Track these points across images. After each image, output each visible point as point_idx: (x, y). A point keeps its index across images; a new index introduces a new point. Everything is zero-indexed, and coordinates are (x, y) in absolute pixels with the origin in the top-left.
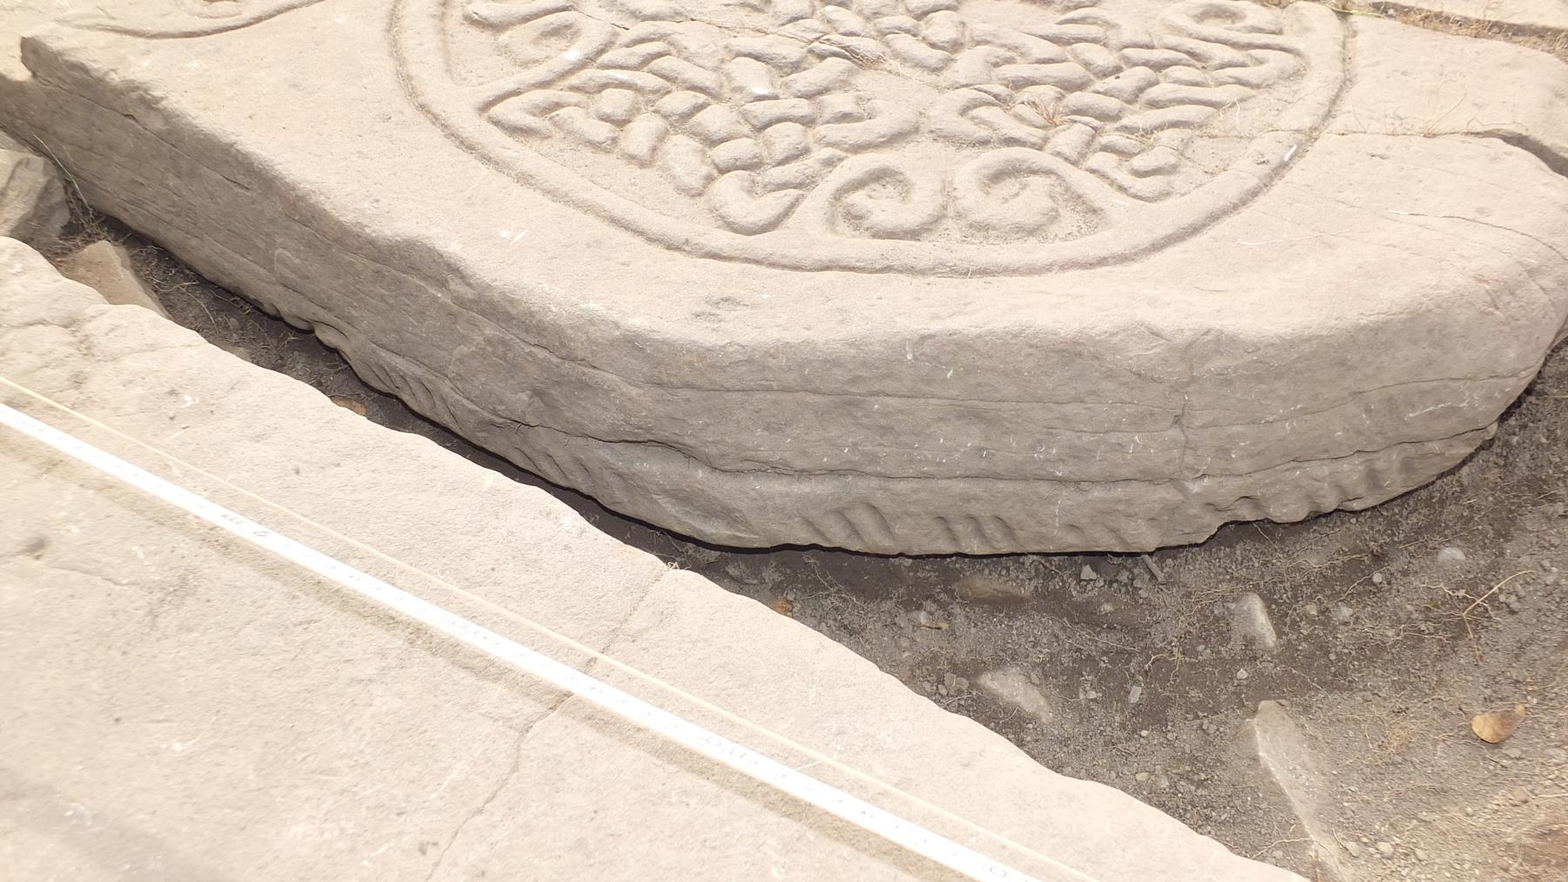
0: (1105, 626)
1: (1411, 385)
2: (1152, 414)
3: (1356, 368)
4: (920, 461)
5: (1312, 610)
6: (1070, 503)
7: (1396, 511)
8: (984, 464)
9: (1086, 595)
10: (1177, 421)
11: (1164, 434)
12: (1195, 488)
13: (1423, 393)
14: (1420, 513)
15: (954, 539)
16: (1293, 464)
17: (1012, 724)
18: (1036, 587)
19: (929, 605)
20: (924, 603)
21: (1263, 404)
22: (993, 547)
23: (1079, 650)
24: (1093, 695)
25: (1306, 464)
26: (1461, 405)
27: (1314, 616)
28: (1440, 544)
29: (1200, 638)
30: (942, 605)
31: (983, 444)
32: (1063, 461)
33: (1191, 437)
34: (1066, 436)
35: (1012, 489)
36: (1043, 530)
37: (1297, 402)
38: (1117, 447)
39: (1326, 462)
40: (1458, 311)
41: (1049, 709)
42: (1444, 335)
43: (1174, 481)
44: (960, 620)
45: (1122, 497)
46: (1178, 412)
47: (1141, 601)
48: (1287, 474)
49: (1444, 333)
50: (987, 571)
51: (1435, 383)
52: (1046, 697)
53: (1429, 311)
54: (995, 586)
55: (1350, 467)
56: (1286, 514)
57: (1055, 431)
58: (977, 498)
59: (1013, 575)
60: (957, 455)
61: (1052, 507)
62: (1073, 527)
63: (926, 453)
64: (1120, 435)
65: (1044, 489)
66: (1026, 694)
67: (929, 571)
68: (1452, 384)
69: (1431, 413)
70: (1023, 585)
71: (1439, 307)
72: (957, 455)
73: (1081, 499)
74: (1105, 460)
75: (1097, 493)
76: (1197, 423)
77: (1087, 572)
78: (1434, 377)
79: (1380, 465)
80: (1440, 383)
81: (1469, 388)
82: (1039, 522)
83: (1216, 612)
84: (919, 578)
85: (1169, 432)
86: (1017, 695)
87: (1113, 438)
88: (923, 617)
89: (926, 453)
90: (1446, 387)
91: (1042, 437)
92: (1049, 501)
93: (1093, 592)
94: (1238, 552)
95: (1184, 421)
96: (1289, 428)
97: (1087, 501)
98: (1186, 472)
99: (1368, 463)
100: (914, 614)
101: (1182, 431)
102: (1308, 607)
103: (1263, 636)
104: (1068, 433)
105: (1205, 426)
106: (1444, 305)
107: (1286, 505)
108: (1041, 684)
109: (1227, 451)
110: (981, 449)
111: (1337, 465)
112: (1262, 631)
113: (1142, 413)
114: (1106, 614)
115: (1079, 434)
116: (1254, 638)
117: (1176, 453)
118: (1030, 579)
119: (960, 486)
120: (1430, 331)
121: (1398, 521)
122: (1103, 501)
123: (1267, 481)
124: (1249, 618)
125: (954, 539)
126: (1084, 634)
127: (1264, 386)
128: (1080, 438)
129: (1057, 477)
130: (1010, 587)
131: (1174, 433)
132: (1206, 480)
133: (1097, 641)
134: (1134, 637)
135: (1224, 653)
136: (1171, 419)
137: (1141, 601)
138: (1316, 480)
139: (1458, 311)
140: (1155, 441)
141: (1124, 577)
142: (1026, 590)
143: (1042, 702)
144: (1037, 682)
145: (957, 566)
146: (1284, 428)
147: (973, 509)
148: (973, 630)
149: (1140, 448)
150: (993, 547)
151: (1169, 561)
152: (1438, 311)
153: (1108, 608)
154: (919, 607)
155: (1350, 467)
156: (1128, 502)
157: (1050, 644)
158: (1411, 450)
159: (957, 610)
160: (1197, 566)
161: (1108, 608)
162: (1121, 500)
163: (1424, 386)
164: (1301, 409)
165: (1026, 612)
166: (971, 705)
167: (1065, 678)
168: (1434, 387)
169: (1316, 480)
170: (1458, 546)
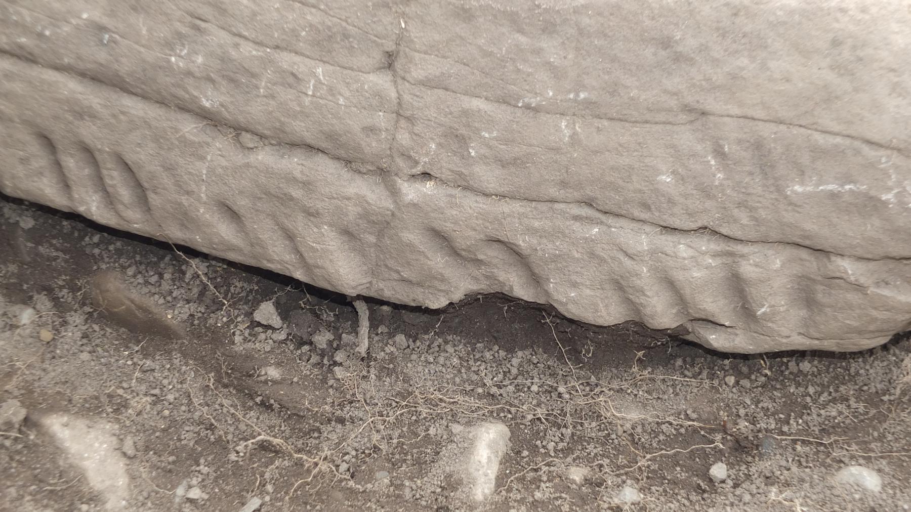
0: (258, 400)
1: (795, 131)
2: (346, 36)
3: (690, 61)
4: (16, 24)
5: (577, 474)
6: (224, 163)
7: (811, 390)
8: (102, 56)
9: (250, 345)
10: (389, 62)
11: (363, 77)
12: (411, 192)
13: (818, 152)
14: (849, 406)
15: (66, 185)
16: (585, 211)
17: (62, 497)
18: (192, 315)
19: (43, 302)
20: (36, 297)
21: (519, 70)
22: (117, 213)
23: (211, 427)
24: (196, 493)
25: (611, 220)
26: (884, 197)
27: (574, 482)
28: (852, 457)
29: (389, 460)
30: (60, 307)
31: (105, 21)
32: (212, 81)
33: (407, 97)
34: (218, 37)
35: (141, 113)
36: (184, 200)
37: (580, 86)
38: (291, 80)
39: (648, 228)
40: (895, 27)
41: (126, 494)
42: (860, 59)
43: (383, 173)
44: (72, 334)
45: (298, 175)
46: (390, 46)
47: (331, 382)
48: (576, 226)
49: (861, 54)
50: (130, 272)
51: (838, 140)
52: (133, 478)
53: (843, 11)
54: (134, 295)
55: (691, 252)
56: (575, 302)
57: (203, 25)
58: (93, 116)
59: (166, 286)
60: (66, 29)
61: (198, 164)
62: (232, 214)
63: (25, 12)
64: (297, 59)
65: (189, 127)
66: (102, 461)
67: (57, 250)
68: (866, 149)
69: (833, 196)
70: (173, 307)
71: (864, 10)
72: (66, 29)
73: (239, 158)
74: (273, 97)
75: (264, 157)
76: (417, 73)
77: (267, 312)
78: (836, 128)
79: (748, 269)
80: (848, 141)
81: (897, 168)
82: (178, 184)
83: (432, 431)
84: (41, 256)
85: (372, 77)
86: (88, 458)
87: (286, 60)
88: (26, 316)
89: (25, 12)
90: (857, 152)
91: (184, 30)
92: (195, 151)
93: (263, 344)
94: (515, 361)
95: (398, 65)
96: (567, 132)
97: (248, 165)
98: (400, 162)
99: (729, 260)
100: (15, 309)
101: (395, 82)
102: (573, 469)
103: (473, 482)
104: (223, 34)
105: (428, 83)
106: (874, 10)
107: (574, 285)
108: (135, 457)
109: (463, 141)
110: (102, 29)
111: (666, 241)
112: (475, 474)
113: (329, 28)
114: (266, 382)
115: (237, 39)
116: (460, 482)
117: (382, 119)
118: (188, 301)
119: (71, 86)
120: (836, 43)
121: (806, 407)
122: (268, 172)
123: (536, 224)
124: (467, 450)
125: (66, 185)
126: (227, 402)
127: (522, 39)
128: (236, 46)
129: (203, 108)
130: (155, 303)
131: (382, 81)
132: (430, 184)
133: (238, 420)
134: (293, 429)
135: (407, 491)
136: (377, 56)
137: (331, 382)
138: (626, 254)
139: (895, 27)
140: (348, 84)
141: (322, 339)
142: (171, 317)
143: (122, 481)
144: (131, 452)
145: (96, 251)
146: (558, 129)
147: (89, 132)
148: (85, 356)
149: (323, 91)
150: (117, 213)
151: (400, 338)
152: (860, 16)
153: (273, 373)
154: (27, 301)
155: (691, 252)
156: (307, 185)
157: (174, 405)
158: (812, 264)
159: (76, 318)
160: (441, 360)
161: (273, 373)
162: (295, 180)
163: (819, 138)
164: (588, 103)
165: (169, 352)
166: (19, 452)
167: (171, 459)
168: (836, 146)
169: (626, 254)
170: (879, 471)
